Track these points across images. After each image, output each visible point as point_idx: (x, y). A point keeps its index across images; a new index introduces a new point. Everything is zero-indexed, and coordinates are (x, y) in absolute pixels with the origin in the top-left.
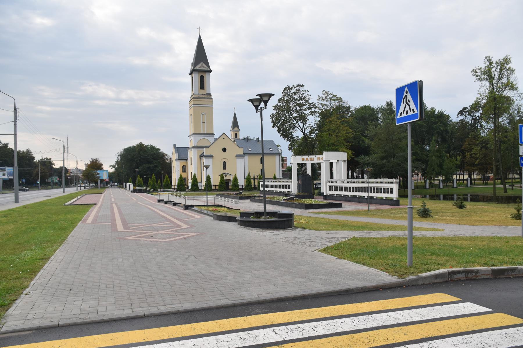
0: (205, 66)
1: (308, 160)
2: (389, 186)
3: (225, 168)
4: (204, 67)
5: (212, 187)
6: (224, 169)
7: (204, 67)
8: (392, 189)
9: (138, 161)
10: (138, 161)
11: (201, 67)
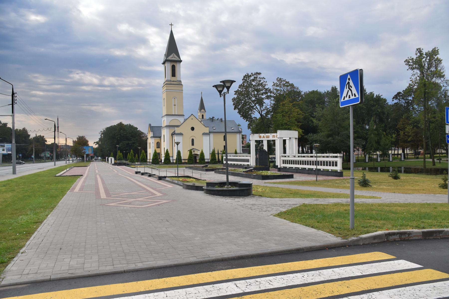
0: (176, 57)
1: (265, 138)
2: (334, 159)
3: (193, 144)
4: (175, 57)
5: (182, 161)
6: (192, 145)
7: (175, 57)
8: (337, 162)
9: (119, 138)
10: (119, 138)
11: (172, 58)
